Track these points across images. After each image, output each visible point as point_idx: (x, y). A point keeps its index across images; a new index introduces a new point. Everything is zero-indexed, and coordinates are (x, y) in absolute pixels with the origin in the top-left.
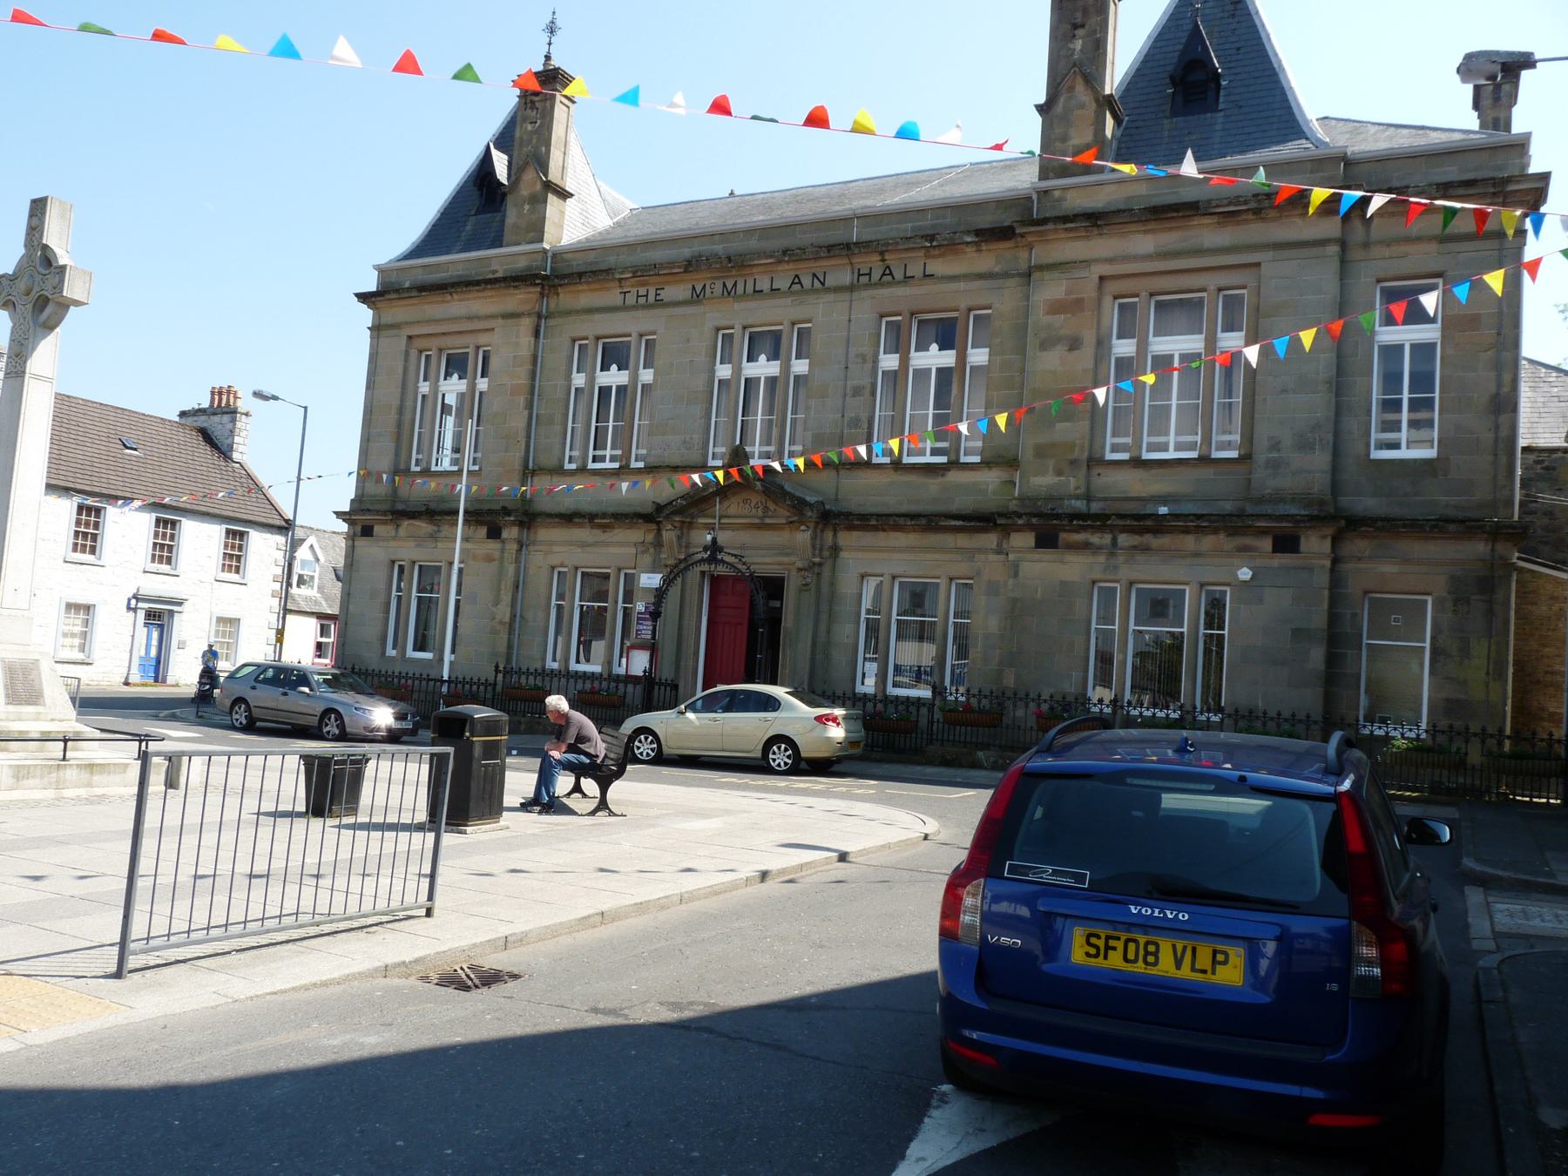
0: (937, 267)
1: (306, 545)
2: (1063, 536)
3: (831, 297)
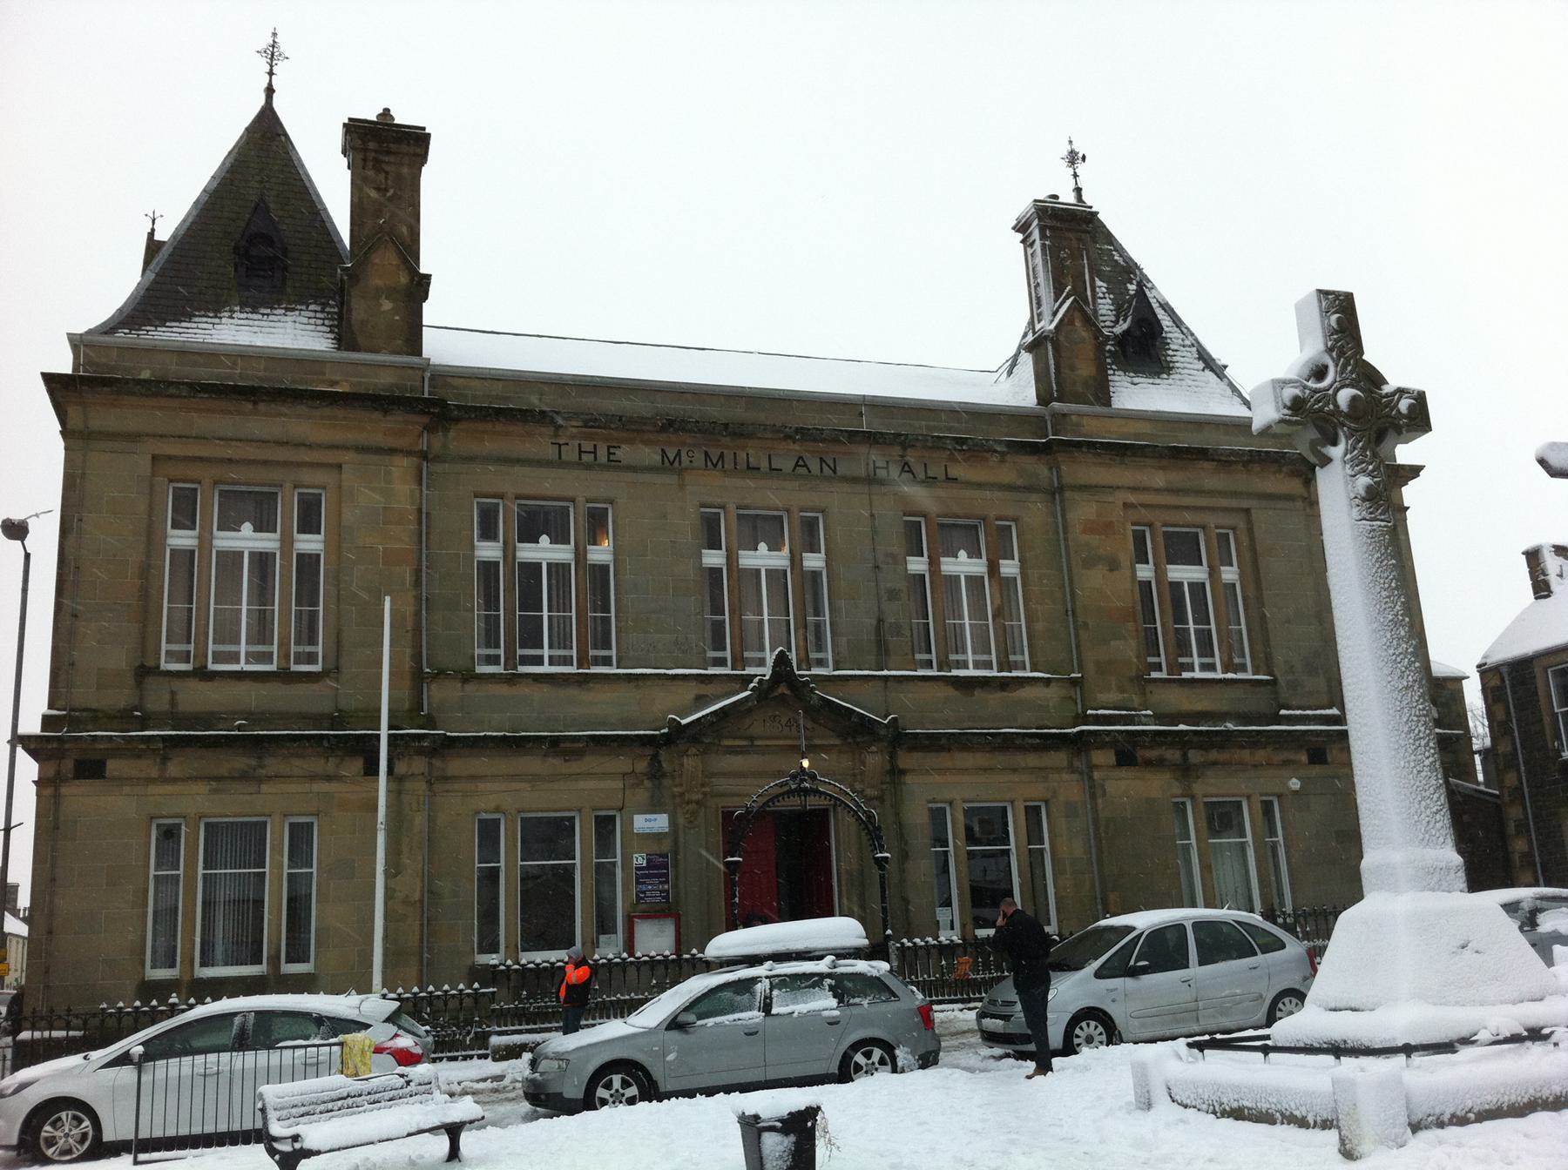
0: (959, 471)
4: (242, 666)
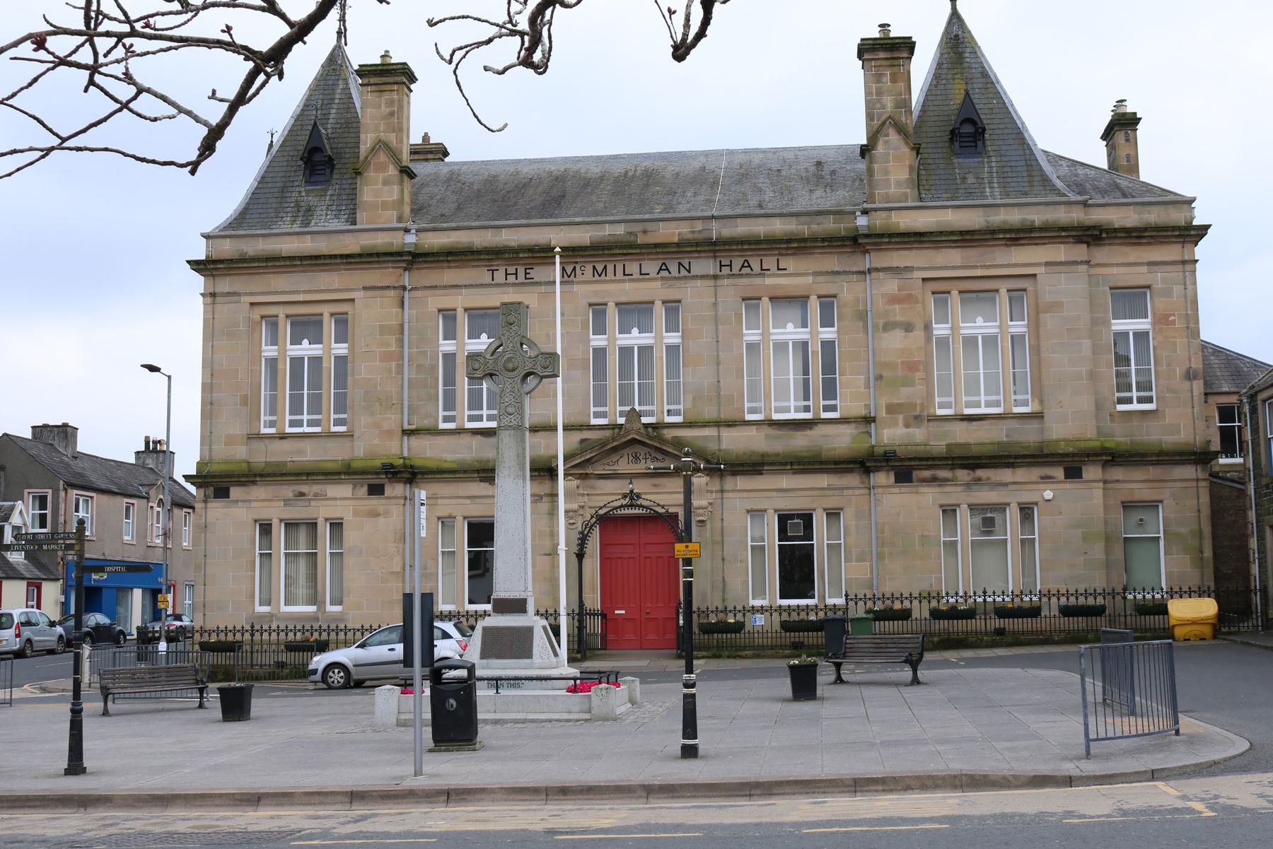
1: (16, 512)
4: (306, 429)
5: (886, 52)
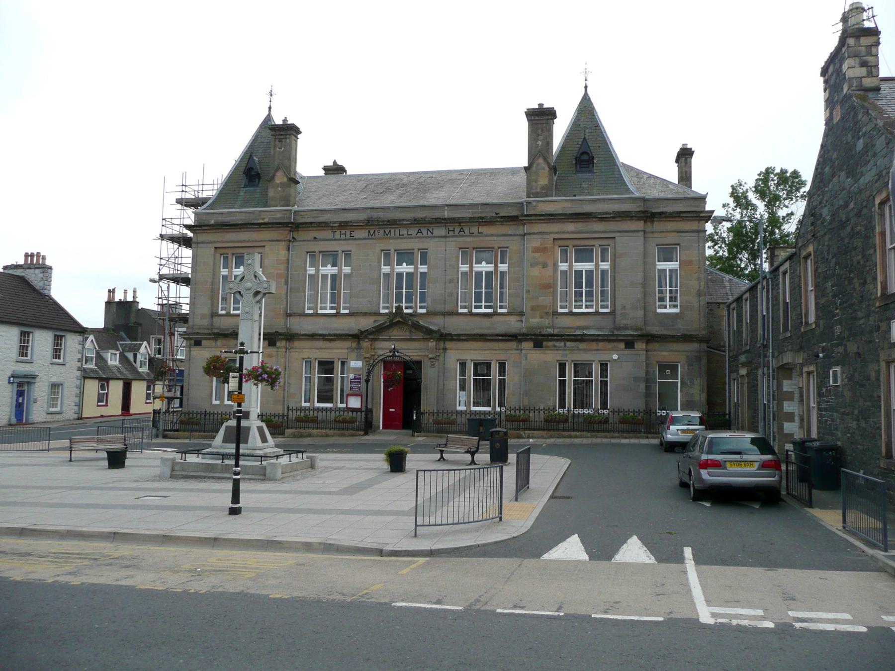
2: (544, 343)
3: (437, 240)
5: (540, 118)
